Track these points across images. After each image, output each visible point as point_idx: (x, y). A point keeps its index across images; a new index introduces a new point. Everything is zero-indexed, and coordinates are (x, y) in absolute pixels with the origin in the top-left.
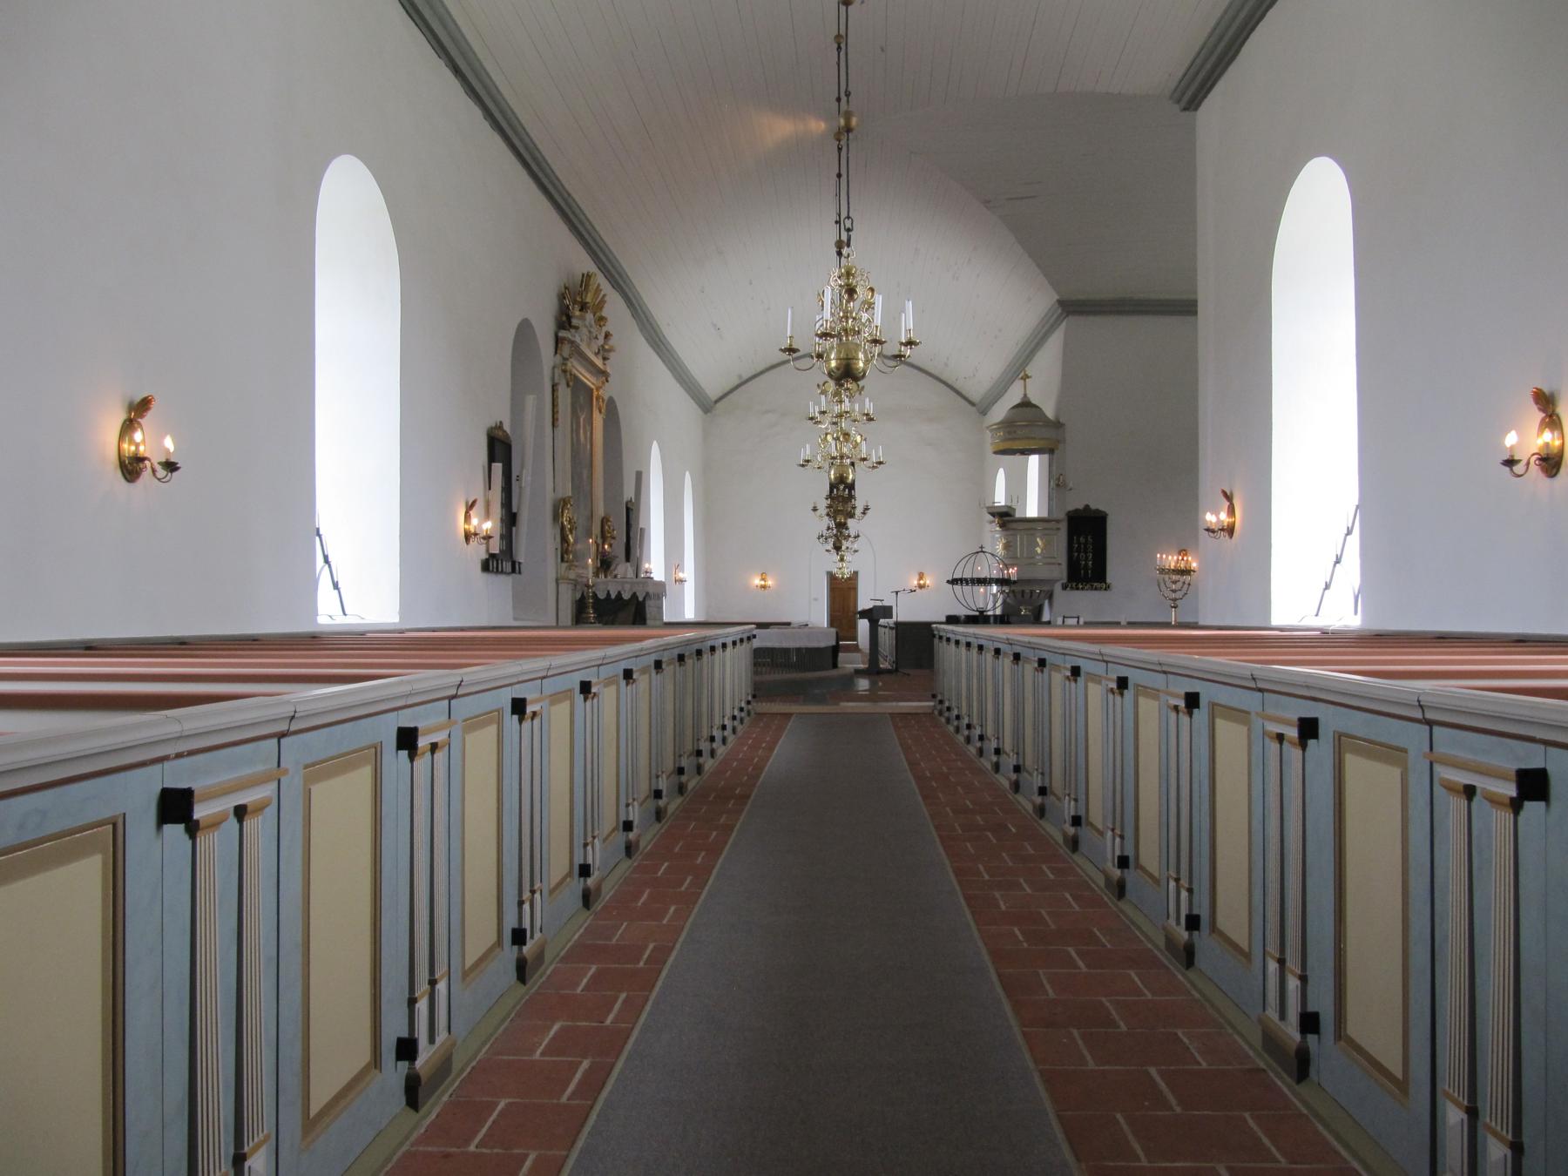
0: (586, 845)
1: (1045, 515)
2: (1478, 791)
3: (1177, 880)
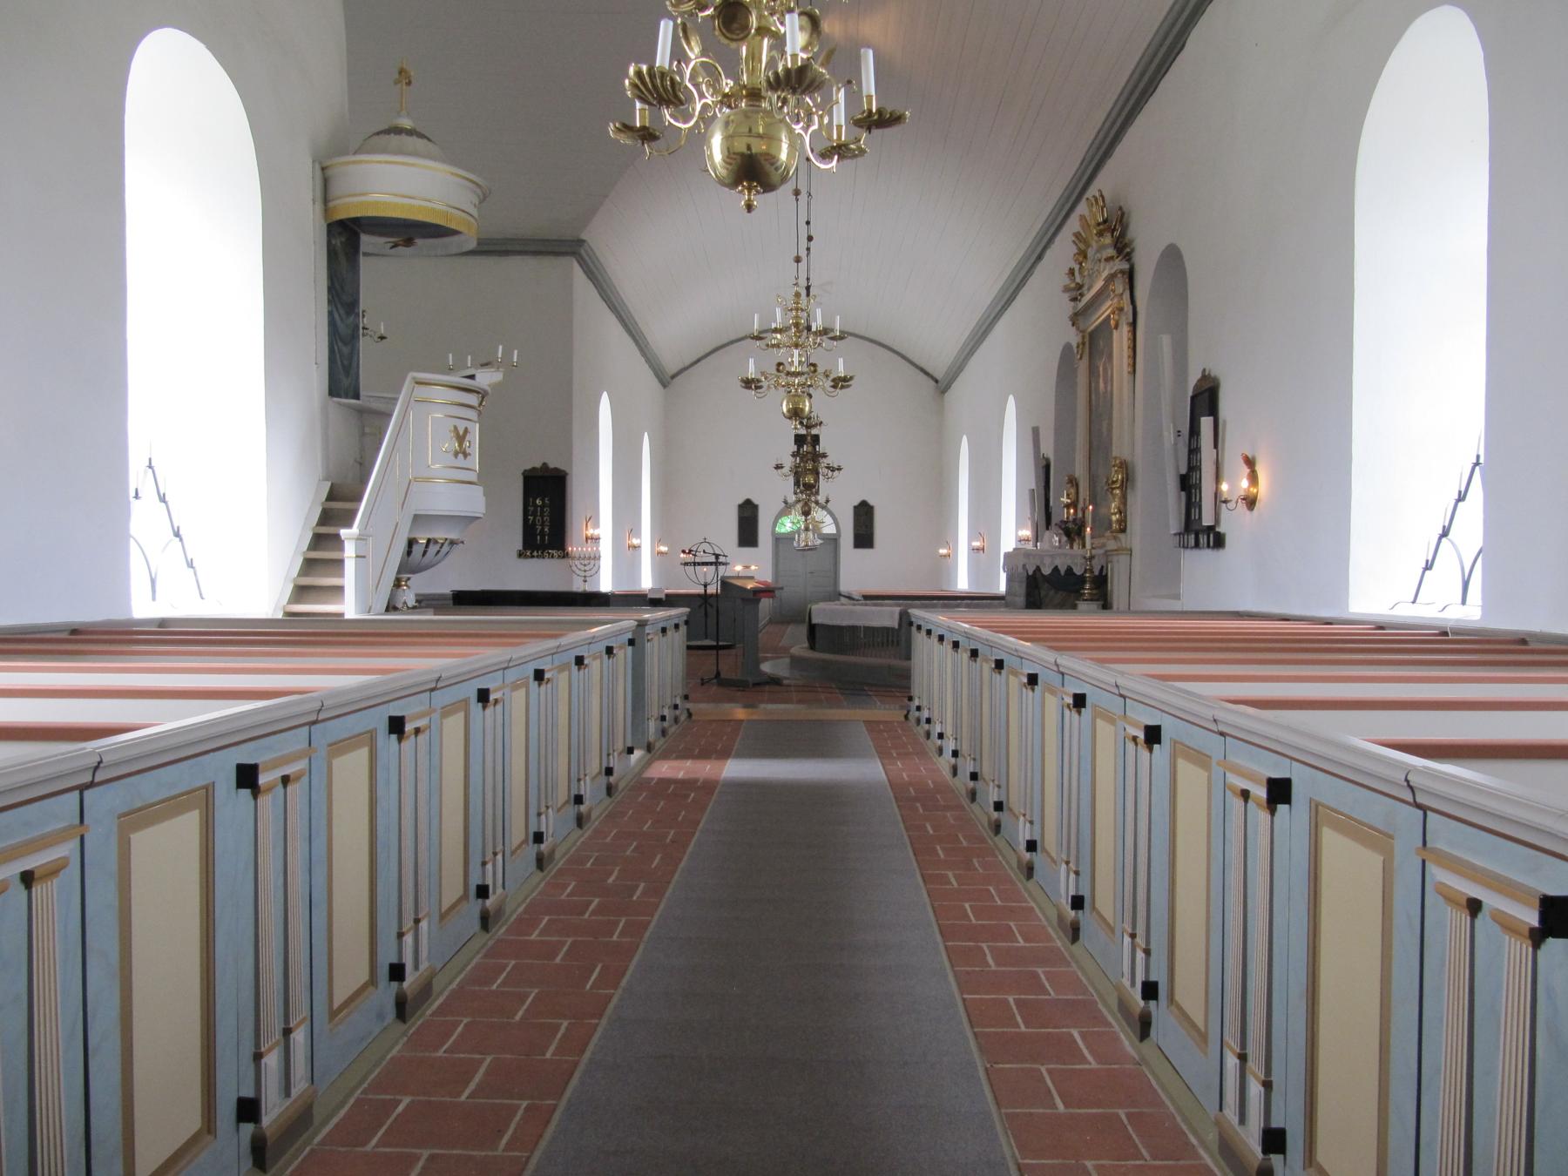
0: (539, 815)
2: (1485, 908)
3: (1133, 936)
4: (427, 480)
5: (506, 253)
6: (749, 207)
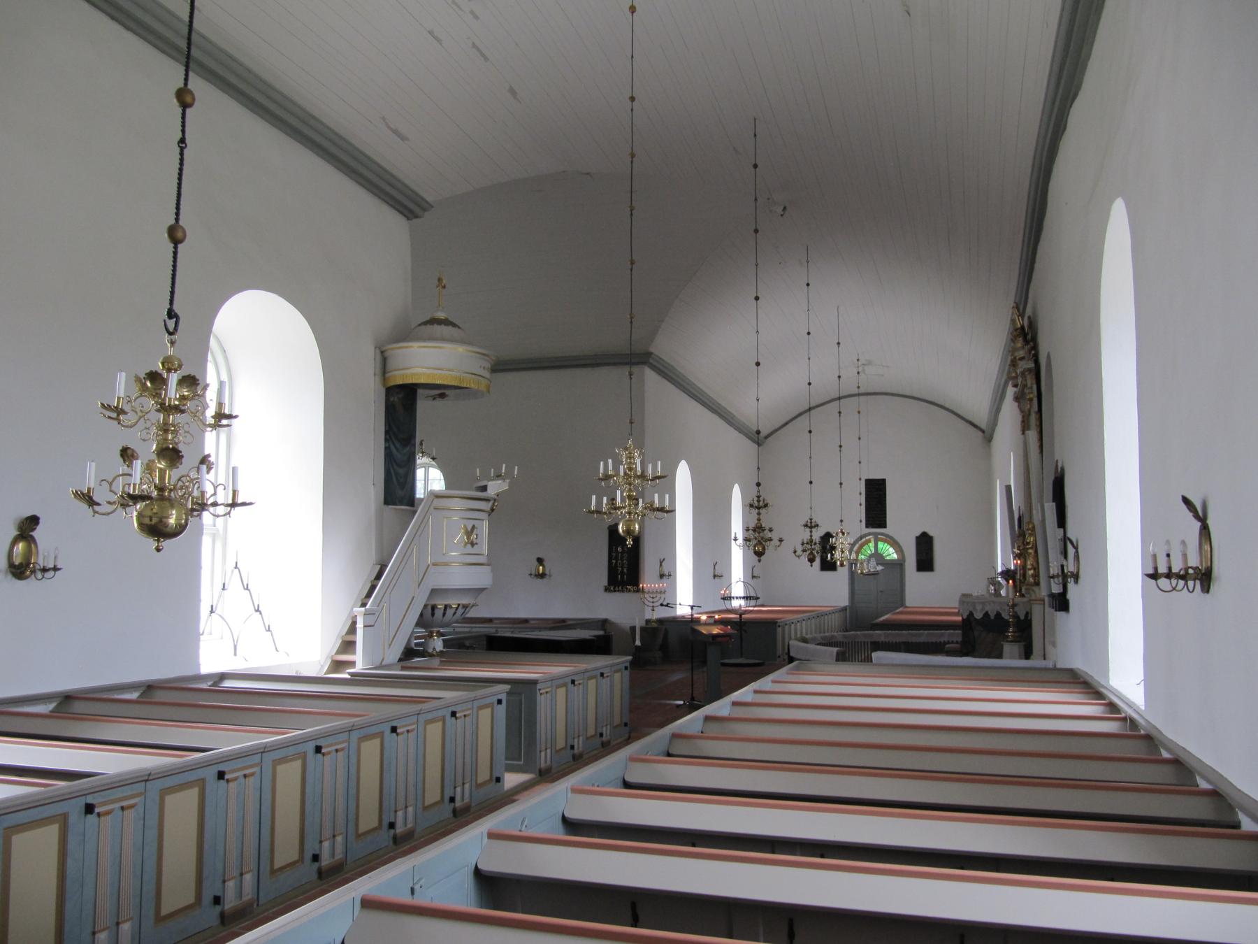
4: (446, 564)
5: (598, 365)
6: (158, 550)
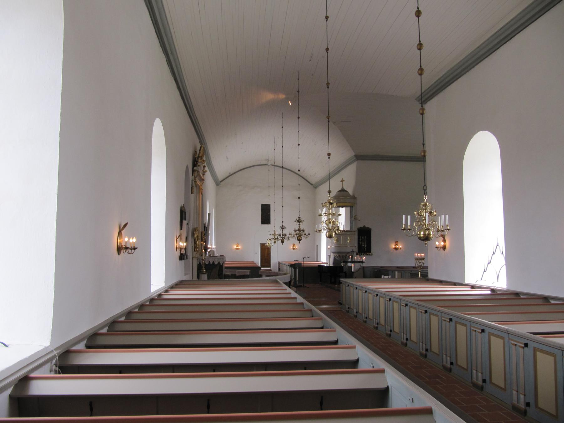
1: (348, 229)
